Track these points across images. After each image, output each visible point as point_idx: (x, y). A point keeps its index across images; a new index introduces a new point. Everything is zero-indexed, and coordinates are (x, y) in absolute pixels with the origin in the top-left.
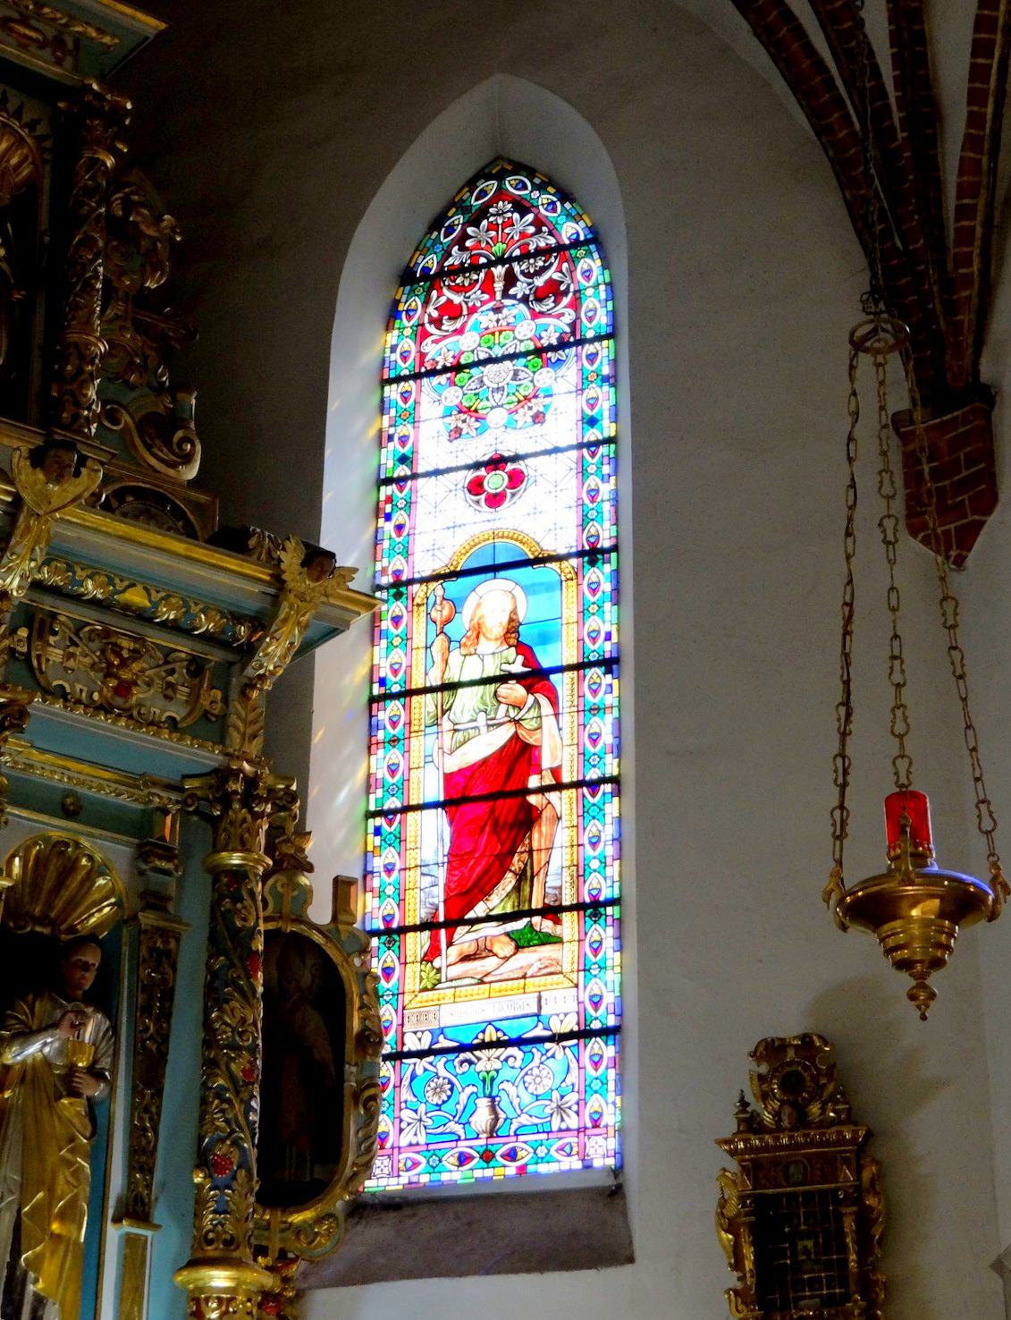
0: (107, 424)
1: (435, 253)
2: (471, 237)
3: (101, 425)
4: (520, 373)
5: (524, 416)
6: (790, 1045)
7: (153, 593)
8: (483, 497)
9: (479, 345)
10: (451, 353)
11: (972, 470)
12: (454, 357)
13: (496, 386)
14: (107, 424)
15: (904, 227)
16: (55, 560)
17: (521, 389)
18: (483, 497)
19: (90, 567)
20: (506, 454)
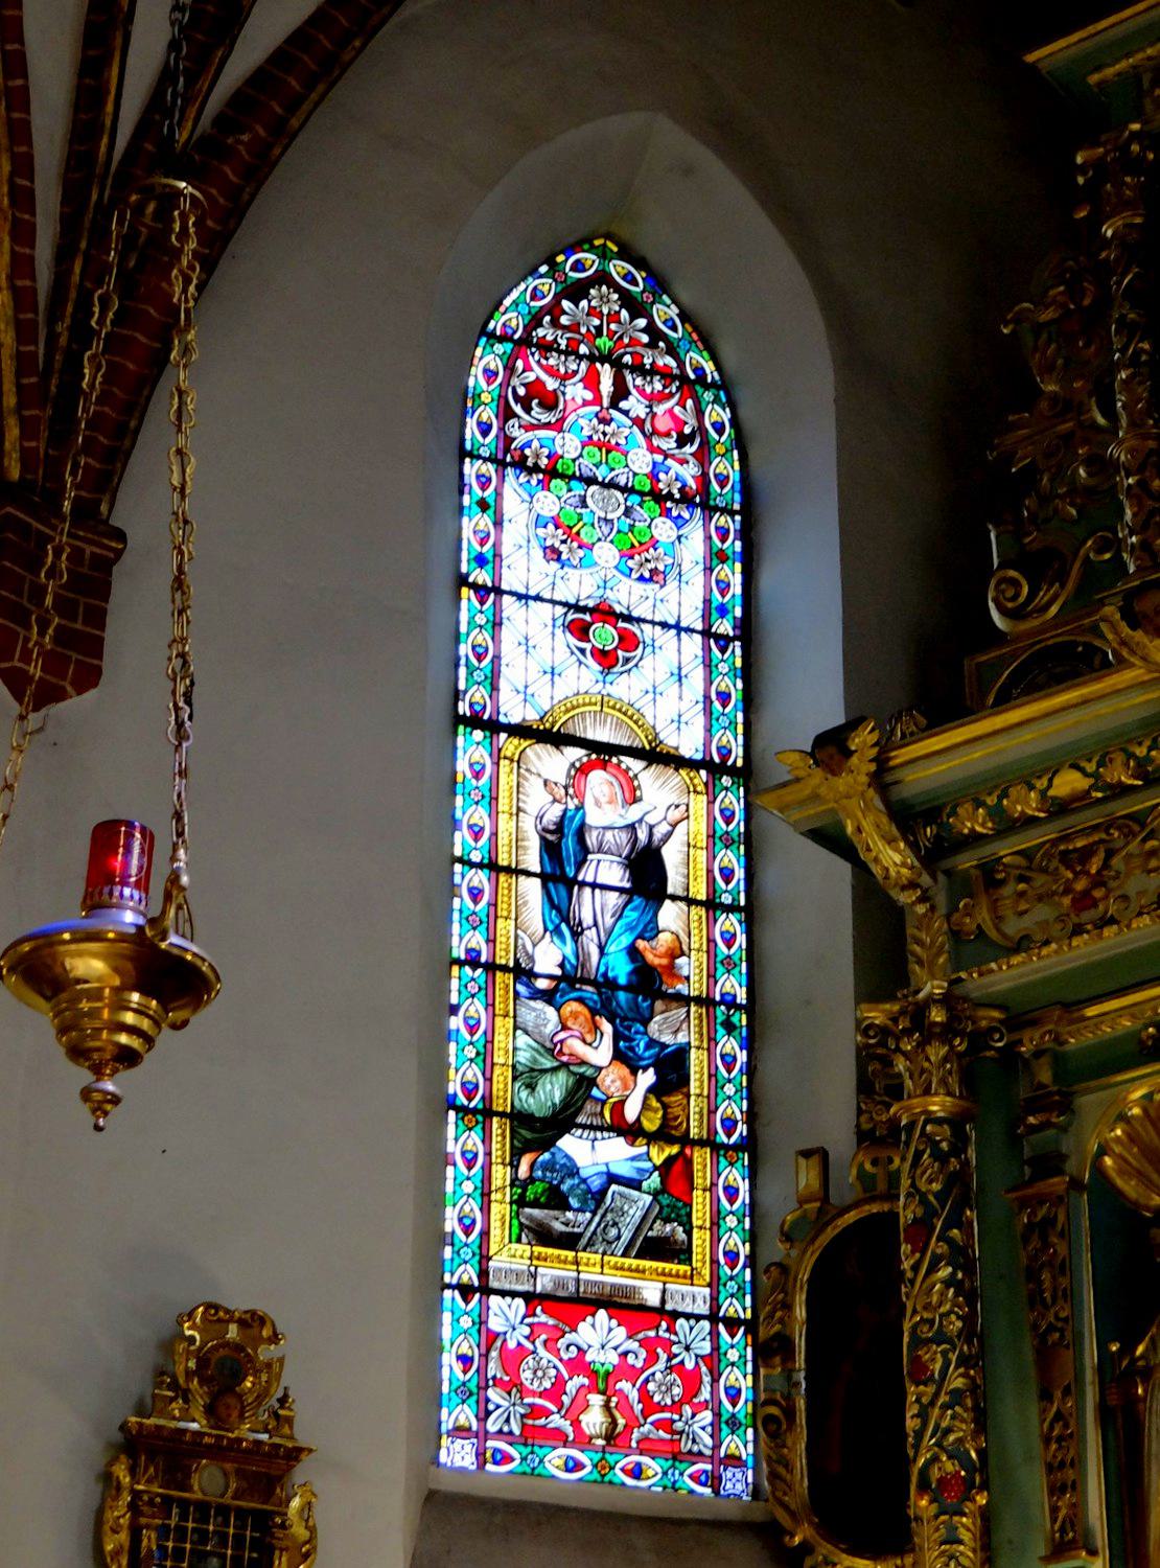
0: (1110, 535)
1: (643, 292)
2: (631, 322)
3: (889, 1049)
4: (609, 526)
5: (554, 536)
6: (938, 833)
7: (1083, 764)
8: (620, 653)
9: (635, 474)
10: (622, 441)
11: (88, 629)
12: (617, 444)
13: (603, 515)
14: (1110, 535)
15: (157, 345)
16: (1010, 786)
17: (588, 528)
18: (620, 653)
19: (996, 787)
20: (618, 609)
